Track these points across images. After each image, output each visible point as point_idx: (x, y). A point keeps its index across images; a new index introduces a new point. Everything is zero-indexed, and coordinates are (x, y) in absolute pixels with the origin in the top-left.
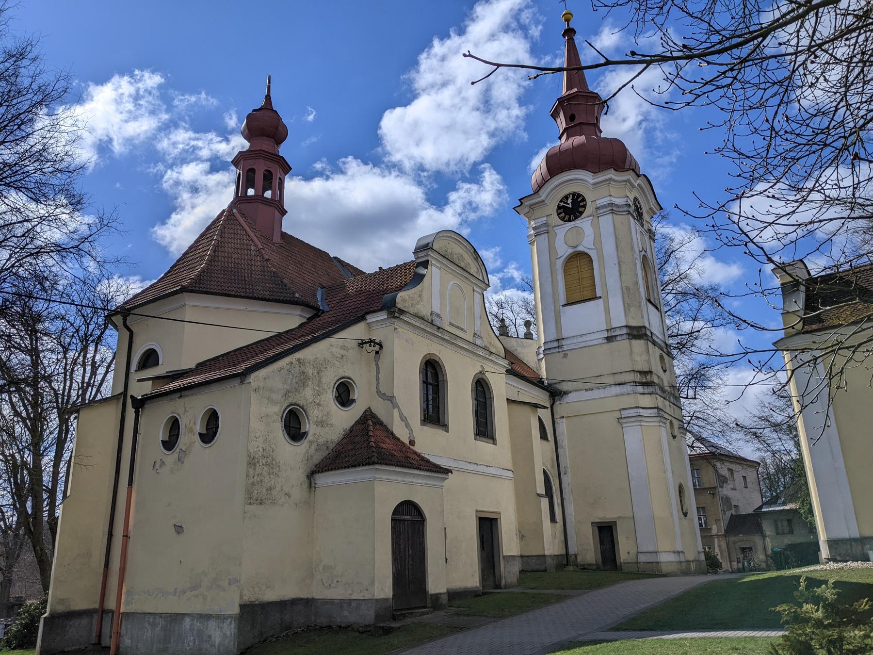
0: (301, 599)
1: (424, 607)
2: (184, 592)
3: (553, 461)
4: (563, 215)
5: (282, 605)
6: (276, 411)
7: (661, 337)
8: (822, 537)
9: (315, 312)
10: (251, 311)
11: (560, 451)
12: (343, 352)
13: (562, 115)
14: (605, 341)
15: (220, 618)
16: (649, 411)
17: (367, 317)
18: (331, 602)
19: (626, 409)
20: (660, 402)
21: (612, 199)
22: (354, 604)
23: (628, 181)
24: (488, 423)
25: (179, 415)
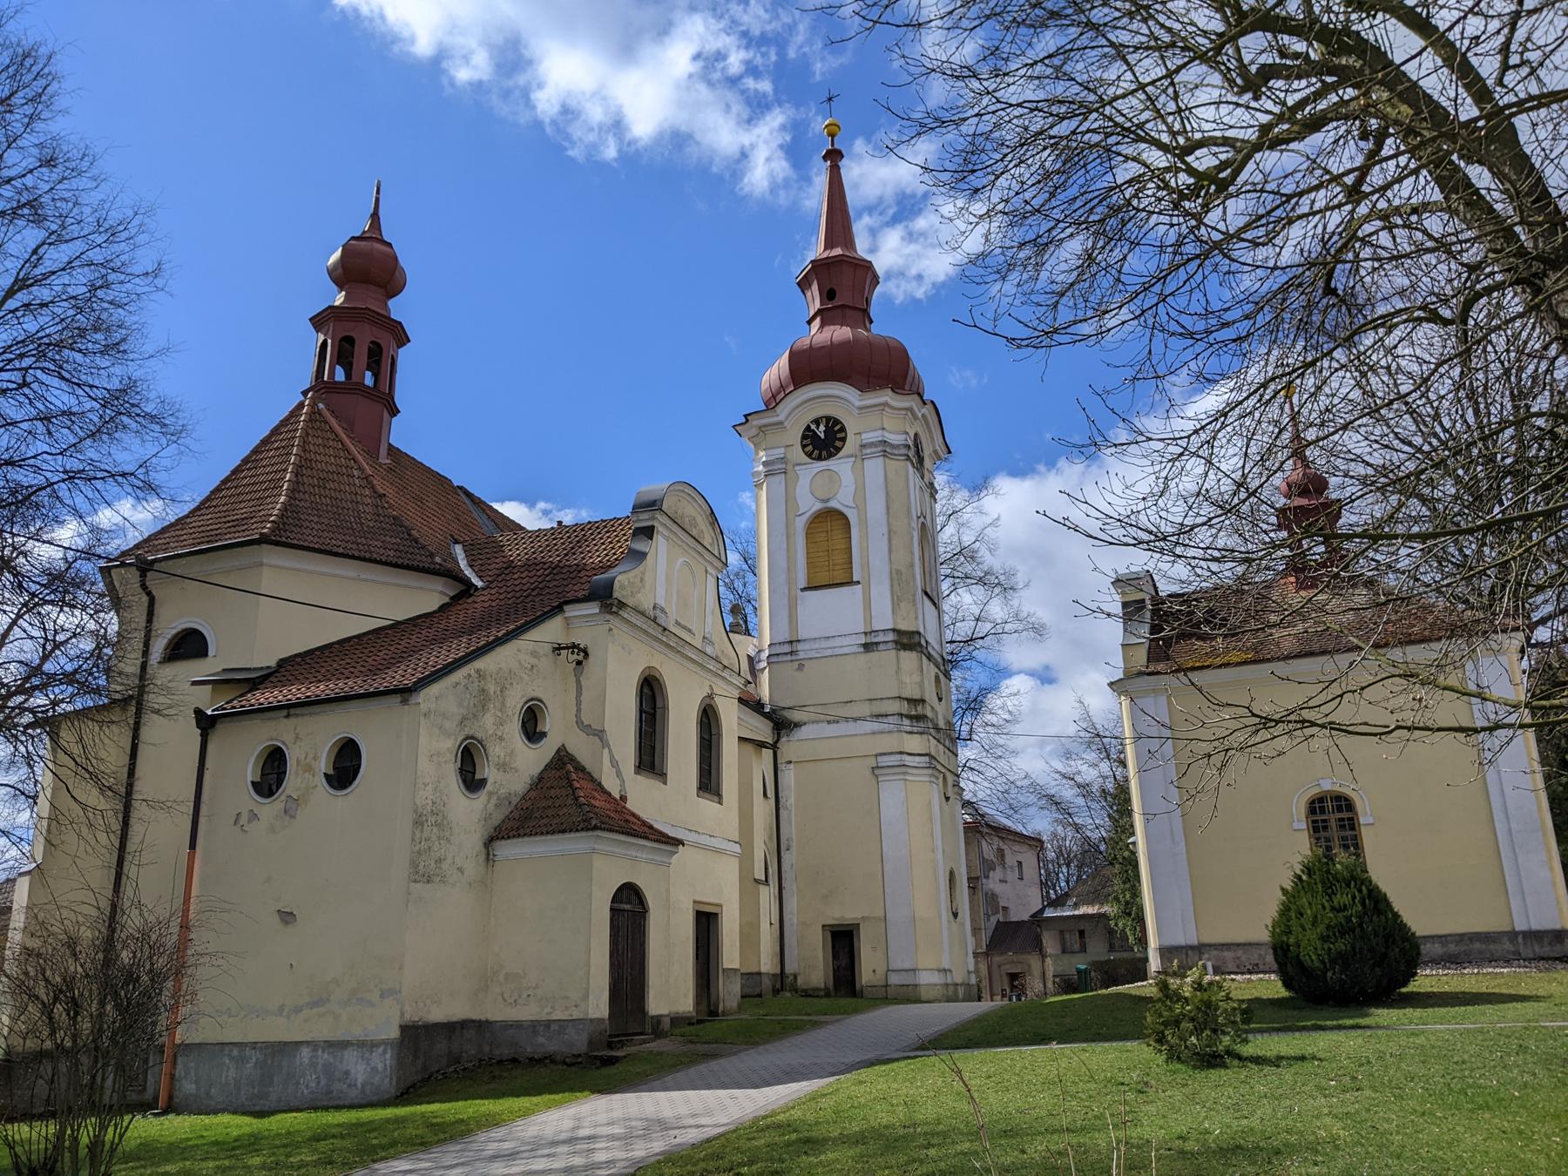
0: (473, 1021)
1: (641, 1034)
2: (298, 1010)
3: (771, 828)
4: (810, 448)
5: (451, 1028)
6: (449, 746)
7: (937, 647)
8: (1153, 943)
9: (463, 587)
10: (366, 580)
11: (783, 813)
12: (533, 661)
13: (815, 287)
14: (862, 650)
15: (366, 1046)
16: (918, 759)
17: (566, 608)
18: (518, 1025)
19: (885, 754)
20: (934, 747)
21: (886, 434)
22: (554, 1027)
23: (910, 409)
24: (713, 772)
25: (284, 743)
